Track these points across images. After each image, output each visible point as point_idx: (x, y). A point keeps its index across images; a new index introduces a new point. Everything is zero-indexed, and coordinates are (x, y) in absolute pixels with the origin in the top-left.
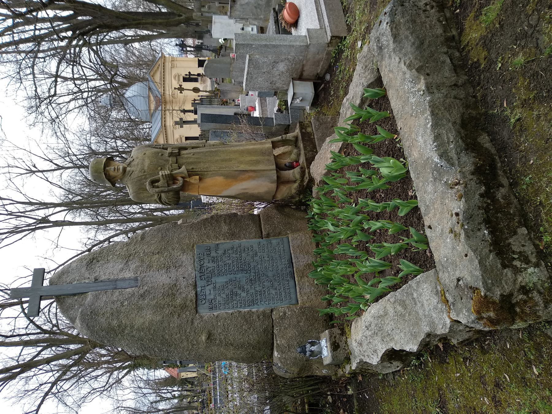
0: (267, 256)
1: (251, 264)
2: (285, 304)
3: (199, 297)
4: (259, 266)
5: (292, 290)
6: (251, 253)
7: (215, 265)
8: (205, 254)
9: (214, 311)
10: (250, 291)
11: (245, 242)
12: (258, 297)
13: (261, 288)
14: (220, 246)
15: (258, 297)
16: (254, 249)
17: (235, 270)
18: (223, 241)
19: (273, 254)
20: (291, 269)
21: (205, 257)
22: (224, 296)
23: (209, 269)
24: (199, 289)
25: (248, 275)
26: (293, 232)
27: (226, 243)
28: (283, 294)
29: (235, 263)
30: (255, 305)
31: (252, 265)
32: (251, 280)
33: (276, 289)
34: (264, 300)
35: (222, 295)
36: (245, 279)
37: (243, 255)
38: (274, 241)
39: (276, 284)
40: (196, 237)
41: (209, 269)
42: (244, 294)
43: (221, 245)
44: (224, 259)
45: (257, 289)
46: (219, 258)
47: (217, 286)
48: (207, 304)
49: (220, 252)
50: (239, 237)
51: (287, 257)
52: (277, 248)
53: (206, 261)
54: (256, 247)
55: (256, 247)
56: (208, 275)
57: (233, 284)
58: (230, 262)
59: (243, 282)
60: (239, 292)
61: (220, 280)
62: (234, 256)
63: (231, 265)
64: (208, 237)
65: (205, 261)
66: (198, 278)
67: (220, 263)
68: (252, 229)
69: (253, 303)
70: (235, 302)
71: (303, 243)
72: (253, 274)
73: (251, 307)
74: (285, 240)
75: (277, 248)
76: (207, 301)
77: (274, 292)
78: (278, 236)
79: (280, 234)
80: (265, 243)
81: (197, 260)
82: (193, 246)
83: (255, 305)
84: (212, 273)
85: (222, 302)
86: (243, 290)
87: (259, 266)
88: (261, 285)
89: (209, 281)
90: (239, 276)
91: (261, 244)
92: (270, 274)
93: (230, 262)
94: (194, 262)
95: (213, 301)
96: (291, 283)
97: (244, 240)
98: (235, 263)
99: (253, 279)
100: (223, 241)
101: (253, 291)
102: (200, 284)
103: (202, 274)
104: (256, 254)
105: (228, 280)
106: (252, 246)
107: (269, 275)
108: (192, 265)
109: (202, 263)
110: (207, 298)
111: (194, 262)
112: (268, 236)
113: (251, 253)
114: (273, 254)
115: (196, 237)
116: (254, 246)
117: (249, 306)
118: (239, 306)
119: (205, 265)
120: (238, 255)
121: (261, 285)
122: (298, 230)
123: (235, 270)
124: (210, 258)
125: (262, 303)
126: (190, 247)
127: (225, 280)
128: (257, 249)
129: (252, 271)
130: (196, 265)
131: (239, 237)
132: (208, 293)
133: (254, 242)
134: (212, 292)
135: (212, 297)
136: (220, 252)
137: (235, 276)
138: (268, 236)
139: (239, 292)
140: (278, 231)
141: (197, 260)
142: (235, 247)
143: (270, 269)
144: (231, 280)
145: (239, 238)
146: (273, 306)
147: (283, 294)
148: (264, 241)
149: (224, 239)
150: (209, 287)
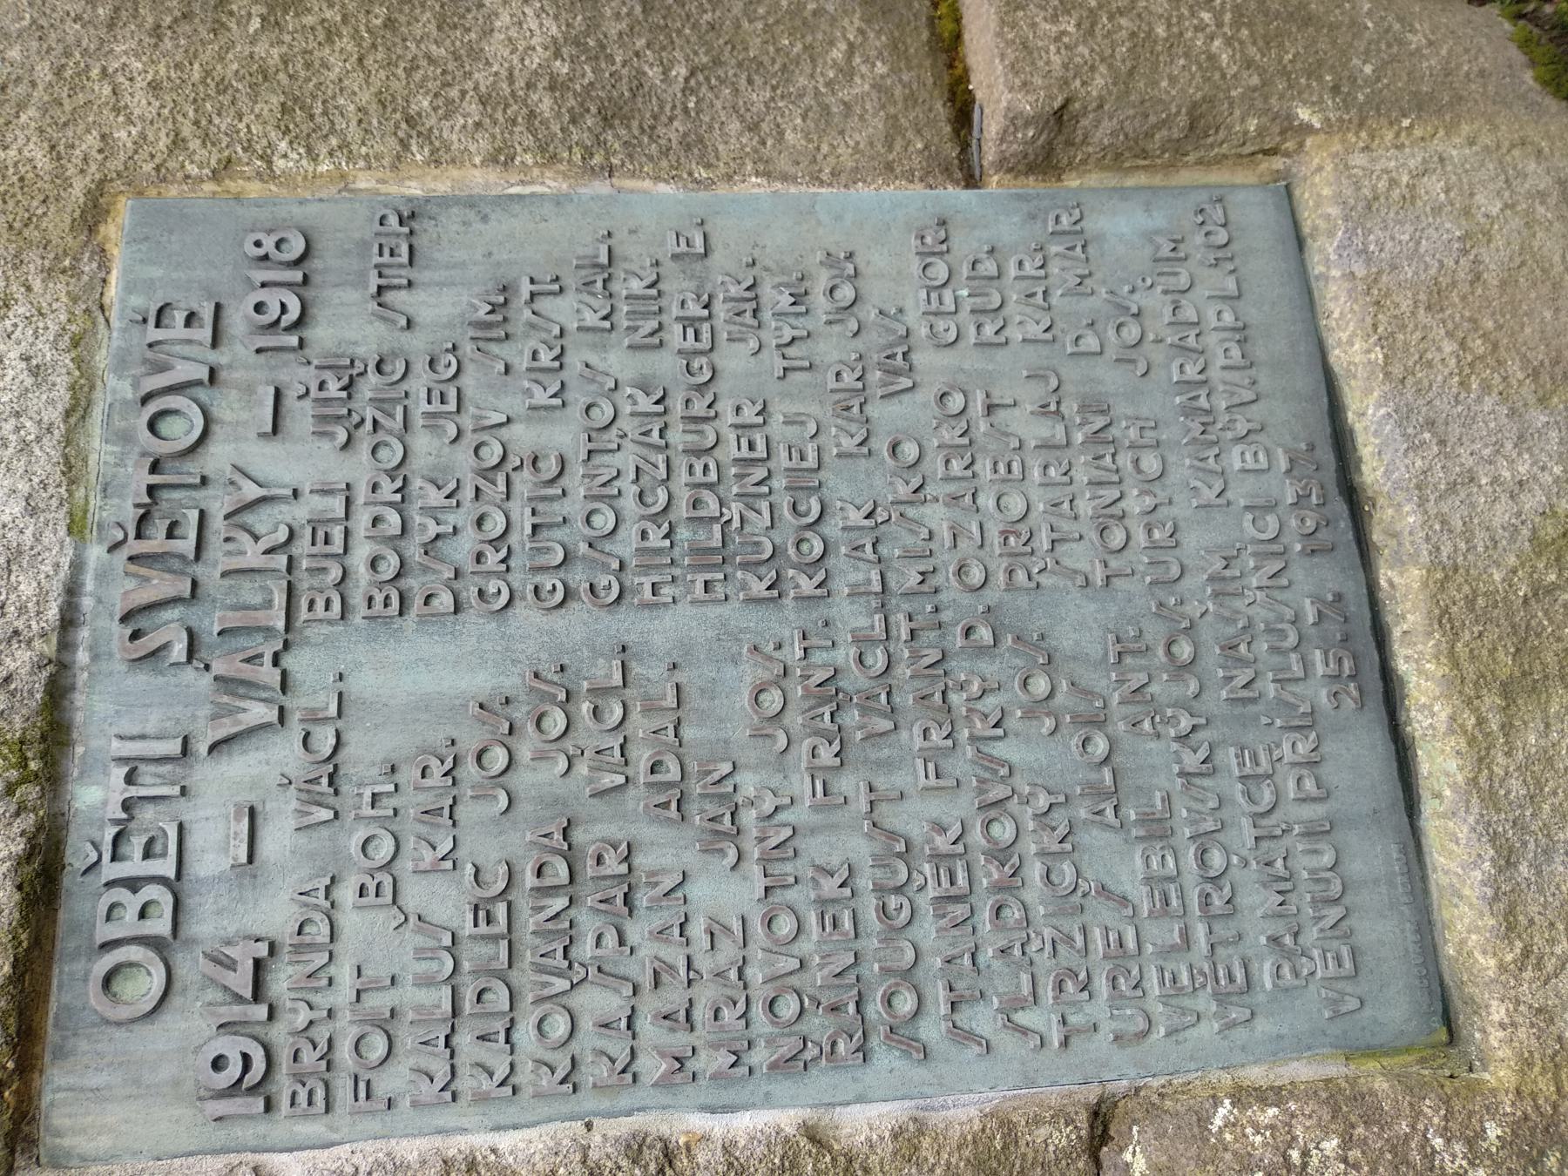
0: (1030, 395)
1: (838, 485)
2: (1278, 1050)
3: (85, 906)
4: (936, 517)
5: (1371, 856)
6: (832, 349)
7: (359, 468)
8: (239, 318)
9: (282, 1126)
10: (815, 849)
11: (759, 215)
12: (927, 930)
13: (961, 807)
14: (447, 240)
15: (927, 930)
16: (877, 294)
17: (626, 545)
18: (481, 179)
19: (1110, 378)
20: (548, 209)
21: (238, 352)
22: (445, 901)
23: (271, 524)
24: (94, 796)
25: (785, 624)
26: (1366, 111)
27: (523, 211)
28: (1257, 900)
29: (627, 460)
30: (886, 1059)
31: (849, 494)
32: (830, 692)
33: (1157, 830)
34: (1003, 981)
35: (415, 895)
36: (749, 673)
37: (734, 360)
38: (1123, 219)
39: (1157, 762)
40: (139, 102)
41: (271, 524)
42: (723, 892)
43: (451, 223)
44: (488, 398)
45: (911, 819)
46: (419, 384)
47: (365, 753)
48: (193, 1026)
49: (440, 306)
50: (695, 144)
51: (1288, 418)
52: (1155, 302)
53: (239, 411)
54: (894, 278)
55: (894, 278)
56: (249, 592)
57: (589, 734)
58: (564, 436)
59: (727, 715)
60: (665, 851)
61: (409, 680)
62: (618, 362)
63: (575, 482)
64: (302, 117)
65: (227, 406)
66: (101, 625)
67: (422, 443)
68: (847, 72)
69: (852, 1022)
70: (598, 1001)
71: (1493, 258)
72: (852, 616)
73: (821, 1081)
74: (1254, 213)
75: (1155, 302)
76: (190, 967)
77: (1129, 871)
78: (1177, 152)
79: (1196, 134)
80: (1009, 229)
81: (116, 388)
82: (93, 214)
83: (886, 1059)
84: (306, 584)
85: (409, 996)
86: (723, 834)
87: (936, 517)
88: (962, 764)
89: (254, 670)
90: (673, 626)
91: (965, 245)
92: (1079, 627)
93: (564, 436)
94: (78, 411)
95: (281, 982)
96: (1358, 754)
97: (755, 186)
98: (627, 460)
99: (855, 680)
100: (481, 179)
101: (860, 848)
102: (116, 713)
103: (162, 585)
104: (898, 363)
105: (512, 682)
106: (846, 265)
107: (1065, 640)
108: (46, 458)
109: (181, 431)
110: (205, 925)
111: (78, 411)
112: (1052, 145)
113: (832, 349)
114: (1110, 378)
115: (139, 102)
116: (874, 260)
117: (791, 1065)
118: (652, 1066)
119: (218, 457)
120: (666, 365)
121: (962, 764)
122: (1421, 105)
123: (626, 545)
124: (297, 376)
125: (982, 1019)
126: (57, 223)
127: (481, 682)
128: (915, 304)
129: (849, 574)
130: (99, 449)
131: (695, 144)
132: (214, 848)
133: (881, 214)
134: (277, 839)
135: (275, 913)
136: (440, 306)
137: (627, 625)
138: (1052, 145)
139: (665, 851)
140: (1176, 85)
141: (116, 388)
142: (635, 253)
143: (1079, 556)
144: (558, 686)
145: (690, 153)
146: (1120, 1074)
147: (1257, 900)
148: (992, 213)
149: (501, 158)
150: (241, 767)
